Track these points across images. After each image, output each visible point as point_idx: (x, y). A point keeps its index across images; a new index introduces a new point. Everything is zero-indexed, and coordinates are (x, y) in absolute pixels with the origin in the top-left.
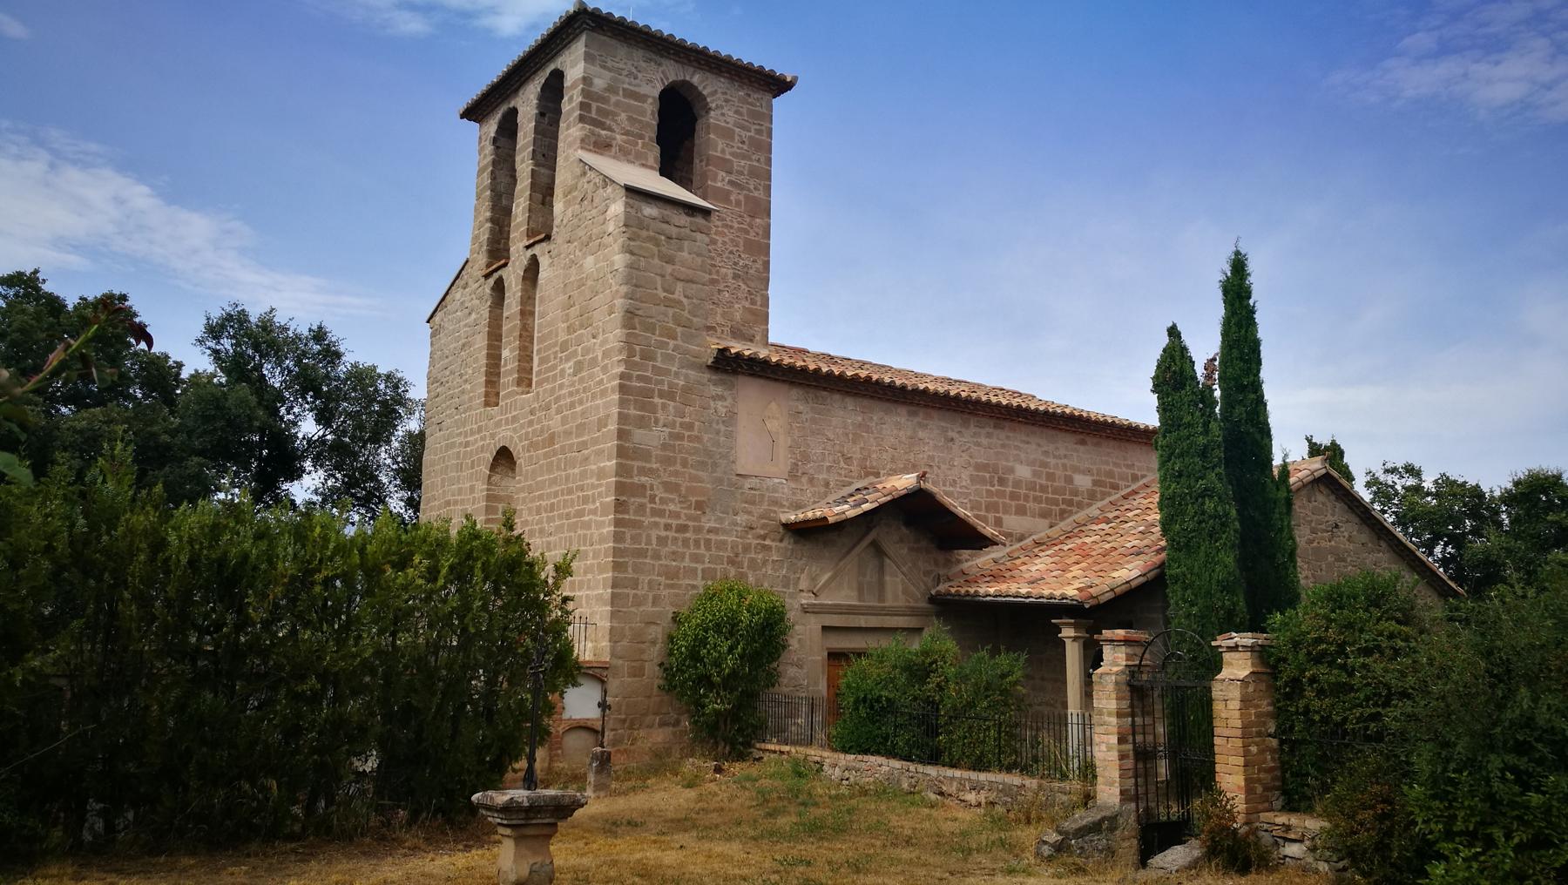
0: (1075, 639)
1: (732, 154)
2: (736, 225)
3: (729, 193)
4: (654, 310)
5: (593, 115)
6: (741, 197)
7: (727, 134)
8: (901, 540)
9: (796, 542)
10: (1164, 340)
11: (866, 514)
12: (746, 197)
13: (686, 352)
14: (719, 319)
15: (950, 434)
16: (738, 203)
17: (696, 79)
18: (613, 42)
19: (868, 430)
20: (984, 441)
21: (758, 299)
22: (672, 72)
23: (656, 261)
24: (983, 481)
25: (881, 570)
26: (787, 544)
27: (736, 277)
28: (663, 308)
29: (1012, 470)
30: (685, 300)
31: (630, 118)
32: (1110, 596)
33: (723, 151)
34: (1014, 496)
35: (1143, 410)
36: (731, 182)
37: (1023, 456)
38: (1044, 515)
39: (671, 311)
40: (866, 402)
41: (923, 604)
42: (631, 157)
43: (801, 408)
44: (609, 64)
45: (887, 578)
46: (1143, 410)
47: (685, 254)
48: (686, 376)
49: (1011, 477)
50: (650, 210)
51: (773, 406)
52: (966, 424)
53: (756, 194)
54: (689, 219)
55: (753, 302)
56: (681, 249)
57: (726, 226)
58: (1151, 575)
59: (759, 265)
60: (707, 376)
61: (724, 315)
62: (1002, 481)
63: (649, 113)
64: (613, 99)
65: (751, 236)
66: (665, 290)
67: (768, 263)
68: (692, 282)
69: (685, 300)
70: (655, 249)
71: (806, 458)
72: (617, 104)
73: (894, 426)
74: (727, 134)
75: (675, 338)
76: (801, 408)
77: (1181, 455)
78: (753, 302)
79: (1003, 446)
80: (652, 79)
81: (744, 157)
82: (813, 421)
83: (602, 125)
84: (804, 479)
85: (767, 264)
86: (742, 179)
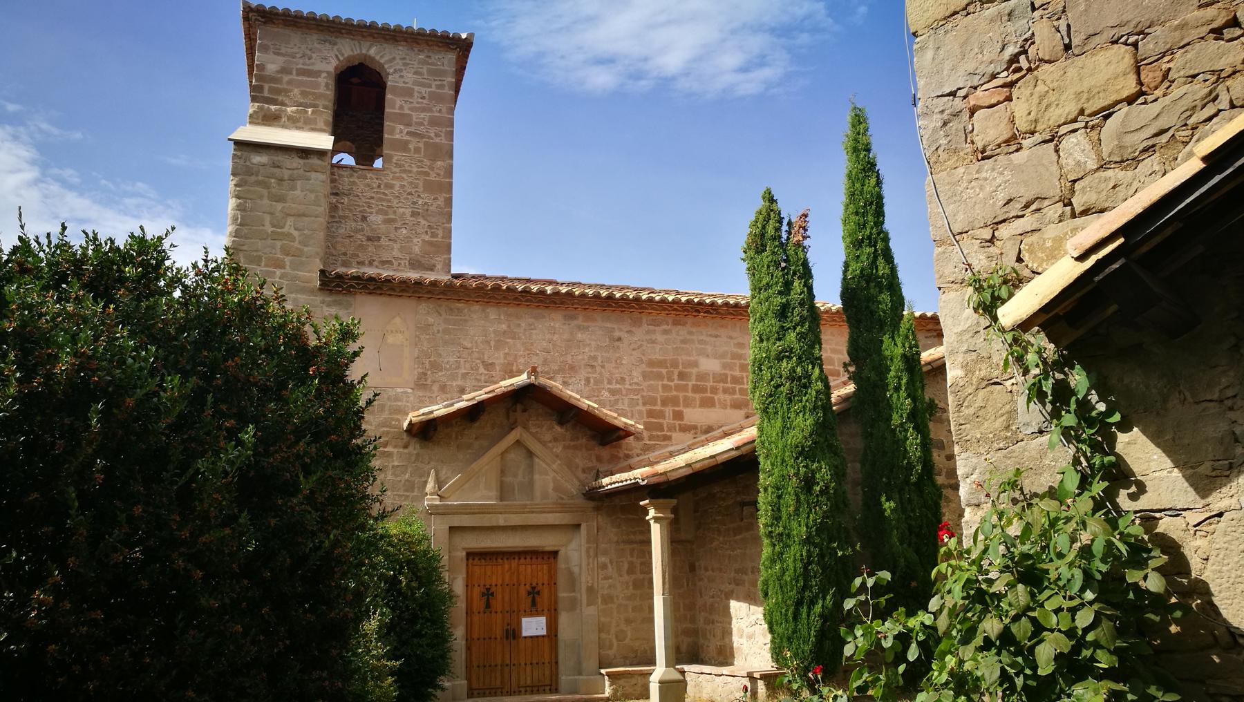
0: (656, 519)
1: (410, 109)
2: (415, 170)
3: (407, 142)
4: (260, 244)
5: (266, 94)
6: (421, 145)
7: (408, 93)
8: (555, 440)
9: (421, 448)
10: (760, 204)
11: (459, 411)
12: (426, 143)
13: (295, 278)
14: (396, 253)
15: (617, 334)
16: (417, 150)
17: (372, 52)
18: (287, 31)
19: (514, 336)
20: (660, 338)
21: (440, 233)
22: (348, 50)
23: (266, 201)
24: (659, 377)
25: (531, 469)
26: (414, 448)
27: (414, 214)
28: (269, 242)
29: (695, 364)
30: (296, 233)
31: (303, 93)
32: (688, 471)
33: (401, 107)
34: (696, 389)
35: (732, 281)
36: (409, 133)
37: (709, 349)
38: (737, 406)
39: (279, 244)
40: (511, 310)
41: (581, 501)
42: (300, 124)
43: (431, 320)
44: (283, 51)
45: (536, 477)
46: (732, 281)
47: (298, 192)
48: (295, 300)
49: (694, 371)
50: (258, 159)
51: (398, 320)
52: (637, 323)
53: (437, 140)
54: (301, 161)
55: (434, 235)
56: (293, 188)
57: (405, 171)
58: (744, 450)
59: (441, 202)
60: (319, 299)
61: (401, 249)
62: (682, 376)
63: (325, 88)
64: (286, 78)
65: (433, 177)
66: (274, 226)
67: (451, 199)
68: (304, 215)
69: (296, 233)
70: (265, 192)
71: (435, 367)
72: (289, 82)
73: (484, 324)
74: (408, 93)
75: (283, 267)
76: (431, 320)
77: (762, 319)
78: (434, 235)
79: (683, 342)
80: (327, 60)
81: (424, 110)
82: (446, 331)
83: (274, 102)
84: (435, 388)
85: (449, 202)
86: (422, 130)
